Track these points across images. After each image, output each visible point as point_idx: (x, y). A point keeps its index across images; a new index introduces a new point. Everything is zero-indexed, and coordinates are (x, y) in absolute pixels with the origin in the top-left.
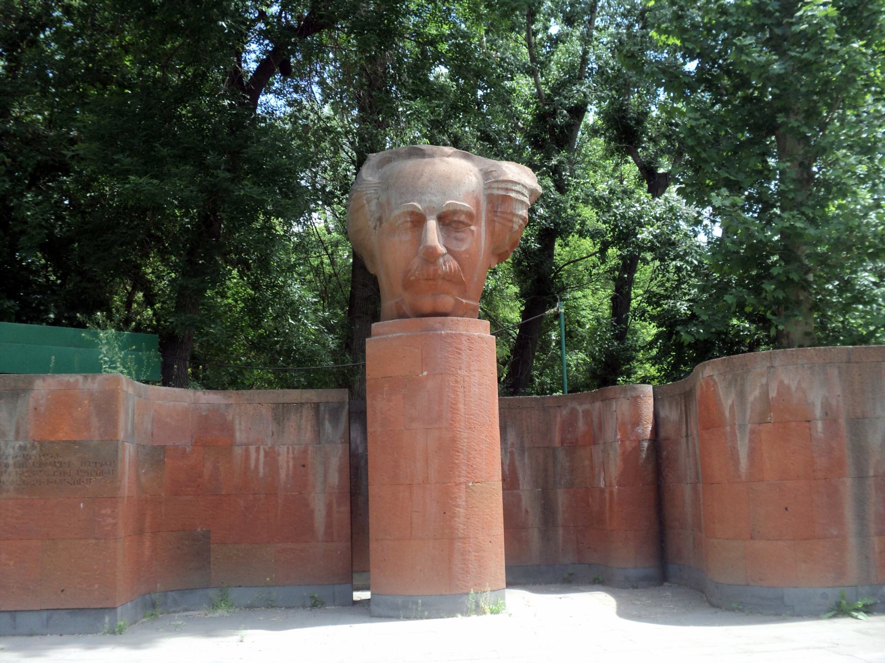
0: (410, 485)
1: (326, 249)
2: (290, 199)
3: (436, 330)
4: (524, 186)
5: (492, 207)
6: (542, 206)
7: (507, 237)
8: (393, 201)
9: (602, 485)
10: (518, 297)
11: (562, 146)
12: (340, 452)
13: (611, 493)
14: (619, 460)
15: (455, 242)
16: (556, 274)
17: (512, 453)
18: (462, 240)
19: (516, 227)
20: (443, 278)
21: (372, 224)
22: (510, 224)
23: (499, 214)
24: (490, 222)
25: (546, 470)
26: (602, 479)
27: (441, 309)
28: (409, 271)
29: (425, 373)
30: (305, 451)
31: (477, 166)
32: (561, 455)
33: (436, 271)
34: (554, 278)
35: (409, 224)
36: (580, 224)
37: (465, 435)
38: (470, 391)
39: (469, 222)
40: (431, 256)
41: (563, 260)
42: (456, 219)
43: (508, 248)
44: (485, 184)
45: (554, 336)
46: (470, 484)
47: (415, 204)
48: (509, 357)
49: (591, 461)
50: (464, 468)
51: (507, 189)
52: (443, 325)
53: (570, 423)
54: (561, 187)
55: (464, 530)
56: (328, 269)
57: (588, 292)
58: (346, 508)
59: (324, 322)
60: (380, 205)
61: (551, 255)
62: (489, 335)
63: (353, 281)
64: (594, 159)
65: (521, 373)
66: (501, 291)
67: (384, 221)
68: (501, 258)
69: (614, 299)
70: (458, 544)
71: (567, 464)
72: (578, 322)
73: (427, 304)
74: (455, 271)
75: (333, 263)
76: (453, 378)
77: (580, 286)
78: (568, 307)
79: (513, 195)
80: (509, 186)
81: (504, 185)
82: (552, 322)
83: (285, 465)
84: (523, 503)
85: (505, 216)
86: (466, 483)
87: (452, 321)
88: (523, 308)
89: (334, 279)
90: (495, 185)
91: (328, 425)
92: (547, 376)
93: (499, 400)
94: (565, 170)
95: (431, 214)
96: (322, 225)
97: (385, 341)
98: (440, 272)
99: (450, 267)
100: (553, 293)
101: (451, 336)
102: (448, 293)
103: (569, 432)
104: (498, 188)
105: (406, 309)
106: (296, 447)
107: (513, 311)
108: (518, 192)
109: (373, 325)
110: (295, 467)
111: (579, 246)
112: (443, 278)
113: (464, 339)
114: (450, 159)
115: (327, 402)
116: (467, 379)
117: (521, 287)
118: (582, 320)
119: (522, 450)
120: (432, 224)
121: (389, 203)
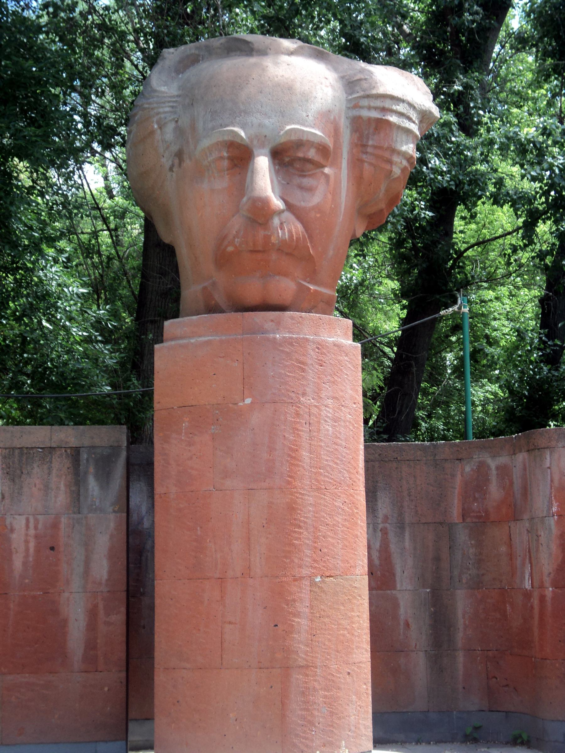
0: (222, 580)
1: (105, 220)
2: (39, 127)
4: (411, 105)
5: (361, 138)
6: (437, 155)
7: (383, 188)
8: (200, 125)
9: (527, 585)
10: (398, 296)
11: (471, 63)
12: (112, 525)
13: (542, 598)
14: (554, 547)
15: (298, 193)
16: (455, 260)
17: (384, 532)
18: (310, 190)
21: (166, 162)
22: (388, 167)
23: (369, 150)
24: (356, 163)
25: (437, 559)
26: (527, 577)
27: (275, 299)
29: (248, 401)
30: (55, 526)
31: (336, 70)
32: (462, 536)
33: (267, 238)
34: (452, 267)
35: (226, 163)
36: (495, 184)
37: (311, 500)
38: (319, 430)
40: (260, 213)
42: (300, 155)
43: (382, 205)
44: (349, 101)
45: (450, 357)
46: (318, 579)
47: (236, 129)
48: (381, 388)
49: (510, 546)
50: (308, 552)
51: (384, 110)
52: (278, 323)
53: (477, 485)
54: (468, 126)
55: (306, 653)
57: (504, 291)
58: (119, 618)
59: (98, 325)
60: (180, 132)
61: (449, 232)
62: (350, 342)
63: (145, 270)
64: (517, 85)
65: (400, 413)
66: (371, 287)
67: (185, 157)
69: (543, 301)
70: (297, 677)
71: (472, 551)
72: (487, 337)
73: (252, 290)
75: (116, 243)
76: (291, 410)
77: (492, 281)
79: (393, 119)
81: (378, 103)
82: (447, 336)
83: (22, 548)
84: (402, 611)
85: (380, 152)
86: (311, 577)
87: (292, 318)
88: (404, 314)
90: (365, 102)
91: (92, 484)
92: (438, 419)
93: (366, 447)
94: (474, 99)
95: (262, 146)
96: (101, 184)
97: (185, 350)
98: (273, 239)
99: (290, 232)
101: (290, 342)
103: (475, 499)
104: (369, 108)
105: (219, 298)
106: (40, 517)
107: (389, 318)
108: (401, 114)
110: (38, 550)
111: (491, 223)
113: (310, 348)
114: (294, 60)
115: (94, 447)
116: (314, 411)
117: (402, 282)
119: (401, 526)
120: (263, 163)
121: (193, 128)
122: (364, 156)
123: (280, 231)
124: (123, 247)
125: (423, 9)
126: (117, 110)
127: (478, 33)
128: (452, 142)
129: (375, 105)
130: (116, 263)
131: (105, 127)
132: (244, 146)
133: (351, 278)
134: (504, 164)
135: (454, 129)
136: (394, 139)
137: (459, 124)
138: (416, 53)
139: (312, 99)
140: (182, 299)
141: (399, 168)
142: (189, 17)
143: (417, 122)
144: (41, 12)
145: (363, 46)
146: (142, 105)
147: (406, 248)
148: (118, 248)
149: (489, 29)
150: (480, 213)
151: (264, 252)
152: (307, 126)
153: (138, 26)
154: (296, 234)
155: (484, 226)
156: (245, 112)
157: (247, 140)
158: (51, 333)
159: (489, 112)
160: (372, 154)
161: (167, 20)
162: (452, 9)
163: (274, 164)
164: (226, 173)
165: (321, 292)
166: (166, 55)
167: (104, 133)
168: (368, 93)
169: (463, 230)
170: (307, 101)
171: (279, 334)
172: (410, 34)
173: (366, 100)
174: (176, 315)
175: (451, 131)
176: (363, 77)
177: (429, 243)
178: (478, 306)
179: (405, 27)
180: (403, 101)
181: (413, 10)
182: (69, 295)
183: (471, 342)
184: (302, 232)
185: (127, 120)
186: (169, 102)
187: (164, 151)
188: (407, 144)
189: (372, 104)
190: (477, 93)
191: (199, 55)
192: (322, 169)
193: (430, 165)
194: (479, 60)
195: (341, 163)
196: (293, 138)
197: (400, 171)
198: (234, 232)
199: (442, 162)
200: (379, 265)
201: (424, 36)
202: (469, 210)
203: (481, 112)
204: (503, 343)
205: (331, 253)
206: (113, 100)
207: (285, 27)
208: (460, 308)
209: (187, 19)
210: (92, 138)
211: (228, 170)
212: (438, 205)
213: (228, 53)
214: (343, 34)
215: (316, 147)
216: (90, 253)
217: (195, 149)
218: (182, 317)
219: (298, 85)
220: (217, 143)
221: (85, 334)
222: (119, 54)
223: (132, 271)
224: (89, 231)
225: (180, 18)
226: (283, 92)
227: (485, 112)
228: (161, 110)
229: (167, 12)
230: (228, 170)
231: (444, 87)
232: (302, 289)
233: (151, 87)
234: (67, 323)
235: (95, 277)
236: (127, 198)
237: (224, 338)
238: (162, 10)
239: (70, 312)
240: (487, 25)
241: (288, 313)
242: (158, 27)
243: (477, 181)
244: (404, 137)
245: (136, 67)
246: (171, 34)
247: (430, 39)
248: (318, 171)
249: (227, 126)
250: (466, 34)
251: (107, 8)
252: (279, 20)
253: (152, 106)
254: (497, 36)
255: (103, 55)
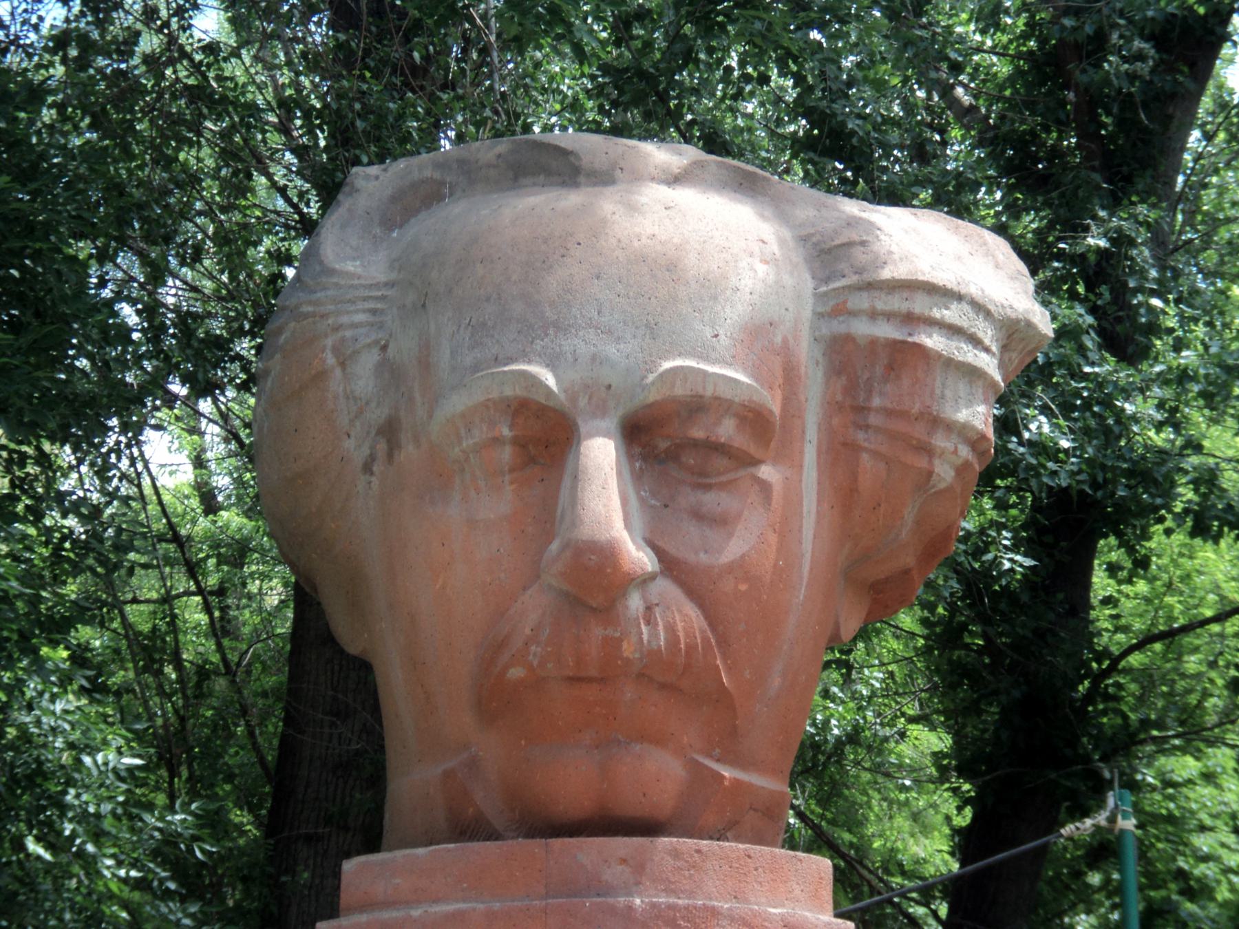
1: (193, 569)
3: (605, 890)
4: (979, 307)
5: (851, 388)
6: (1045, 410)
7: (909, 515)
8: (443, 357)
11: (1129, 179)
15: (692, 530)
18: (722, 522)
19: (944, 473)
20: (642, 677)
21: (355, 448)
22: (922, 462)
23: (874, 419)
24: (840, 453)
27: (630, 804)
28: (502, 644)
34: (1089, 698)
35: (506, 454)
36: (1196, 483)
39: (752, 449)
40: (593, 582)
41: (1125, 629)
42: (698, 433)
44: (819, 297)
51: (911, 320)
52: (639, 868)
54: (1126, 337)
56: (196, 646)
59: (168, 850)
60: (390, 372)
62: (827, 917)
63: (293, 697)
68: (881, 600)
72: (1182, 875)
73: (571, 780)
74: (691, 648)
75: (221, 629)
77: (1195, 735)
78: (1146, 820)
79: (934, 341)
80: (920, 304)
81: (896, 303)
82: (1078, 875)
85: (899, 426)
87: (676, 854)
88: (964, 819)
89: (220, 684)
90: (862, 301)
95: (600, 410)
96: (187, 474)
98: (628, 650)
99: (671, 629)
100: (1087, 759)
102: (659, 740)
104: (873, 315)
105: (486, 800)
107: (926, 830)
108: (954, 331)
109: (349, 866)
111: (1186, 578)
112: (642, 677)
114: (686, 196)
117: (958, 736)
118: (1202, 870)
120: (601, 453)
121: (425, 364)
122: (861, 436)
123: (644, 628)
124: (237, 638)
125: (1005, 47)
126: (231, 297)
127: (1145, 106)
128: (1085, 377)
129: (887, 308)
130: (220, 684)
131: (202, 341)
132: (554, 410)
133: (826, 722)
134: (1215, 431)
135: (1089, 344)
136: (938, 392)
137: (1101, 331)
138: (988, 155)
139: (728, 293)
140: (387, 807)
141: (949, 463)
142: (418, 72)
143: (994, 349)
144: (47, 56)
145: (855, 141)
146: (297, 307)
147: (967, 647)
148: (226, 642)
149: (1173, 96)
150: (1159, 556)
151: (602, 680)
152: (714, 362)
153: (289, 92)
154: (687, 635)
155: (1169, 586)
156: (557, 326)
157: (562, 397)
158: (47, 872)
159: (1178, 301)
160: (878, 430)
161: (362, 78)
162: (1077, 46)
163: (631, 457)
164: (507, 478)
165: (750, 785)
166: (360, 183)
167: (198, 358)
168: (867, 277)
169: (1116, 597)
170: (715, 298)
171: (640, 894)
172: (973, 109)
173: (865, 294)
174: (372, 842)
175: (1082, 350)
176: (857, 238)
177: (1030, 635)
178: (1158, 797)
179: (960, 91)
180: (959, 297)
181: (979, 50)
182: (95, 772)
183: (1141, 889)
184: (702, 632)
185: (260, 322)
186: (365, 299)
187: (351, 421)
188: (969, 404)
189: (880, 306)
190: (1143, 254)
191: (442, 183)
192: (752, 470)
193: (1026, 435)
194: (1149, 172)
195: (802, 452)
196: (679, 391)
197: (953, 474)
198: (528, 631)
199: (1057, 426)
200: (892, 690)
201: (1010, 114)
202: (1131, 550)
203: (1156, 302)
204: (1223, 894)
205: (776, 682)
206: (222, 272)
207: (657, 93)
208: (1112, 820)
209: (414, 77)
210: (169, 367)
211: (512, 470)
212: (1049, 539)
213: (516, 178)
214: (801, 108)
215: (737, 415)
216: (153, 661)
217: (430, 417)
218: (390, 849)
219: (691, 260)
220: (485, 405)
221: (133, 873)
222: (242, 161)
223: (260, 702)
224: (154, 595)
225: (394, 72)
226: (654, 276)
227: (1166, 302)
228: (345, 319)
229: (363, 59)
230: (512, 470)
231: (1059, 239)
232: (701, 779)
233: (321, 263)
234: (90, 848)
235: (166, 720)
236: (248, 514)
237: (497, 906)
238: (352, 52)
239: (98, 816)
240: (1168, 87)
241: (665, 841)
242: (339, 96)
243: (1153, 476)
244: (962, 388)
245: (282, 191)
246: (372, 112)
247: (1023, 122)
248: (741, 473)
249: (511, 360)
250: (1115, 110)
251: (211, 49)
252: (642, 74)
253: (322, 309)
254: (1192, 114)
255: (199, 160)
